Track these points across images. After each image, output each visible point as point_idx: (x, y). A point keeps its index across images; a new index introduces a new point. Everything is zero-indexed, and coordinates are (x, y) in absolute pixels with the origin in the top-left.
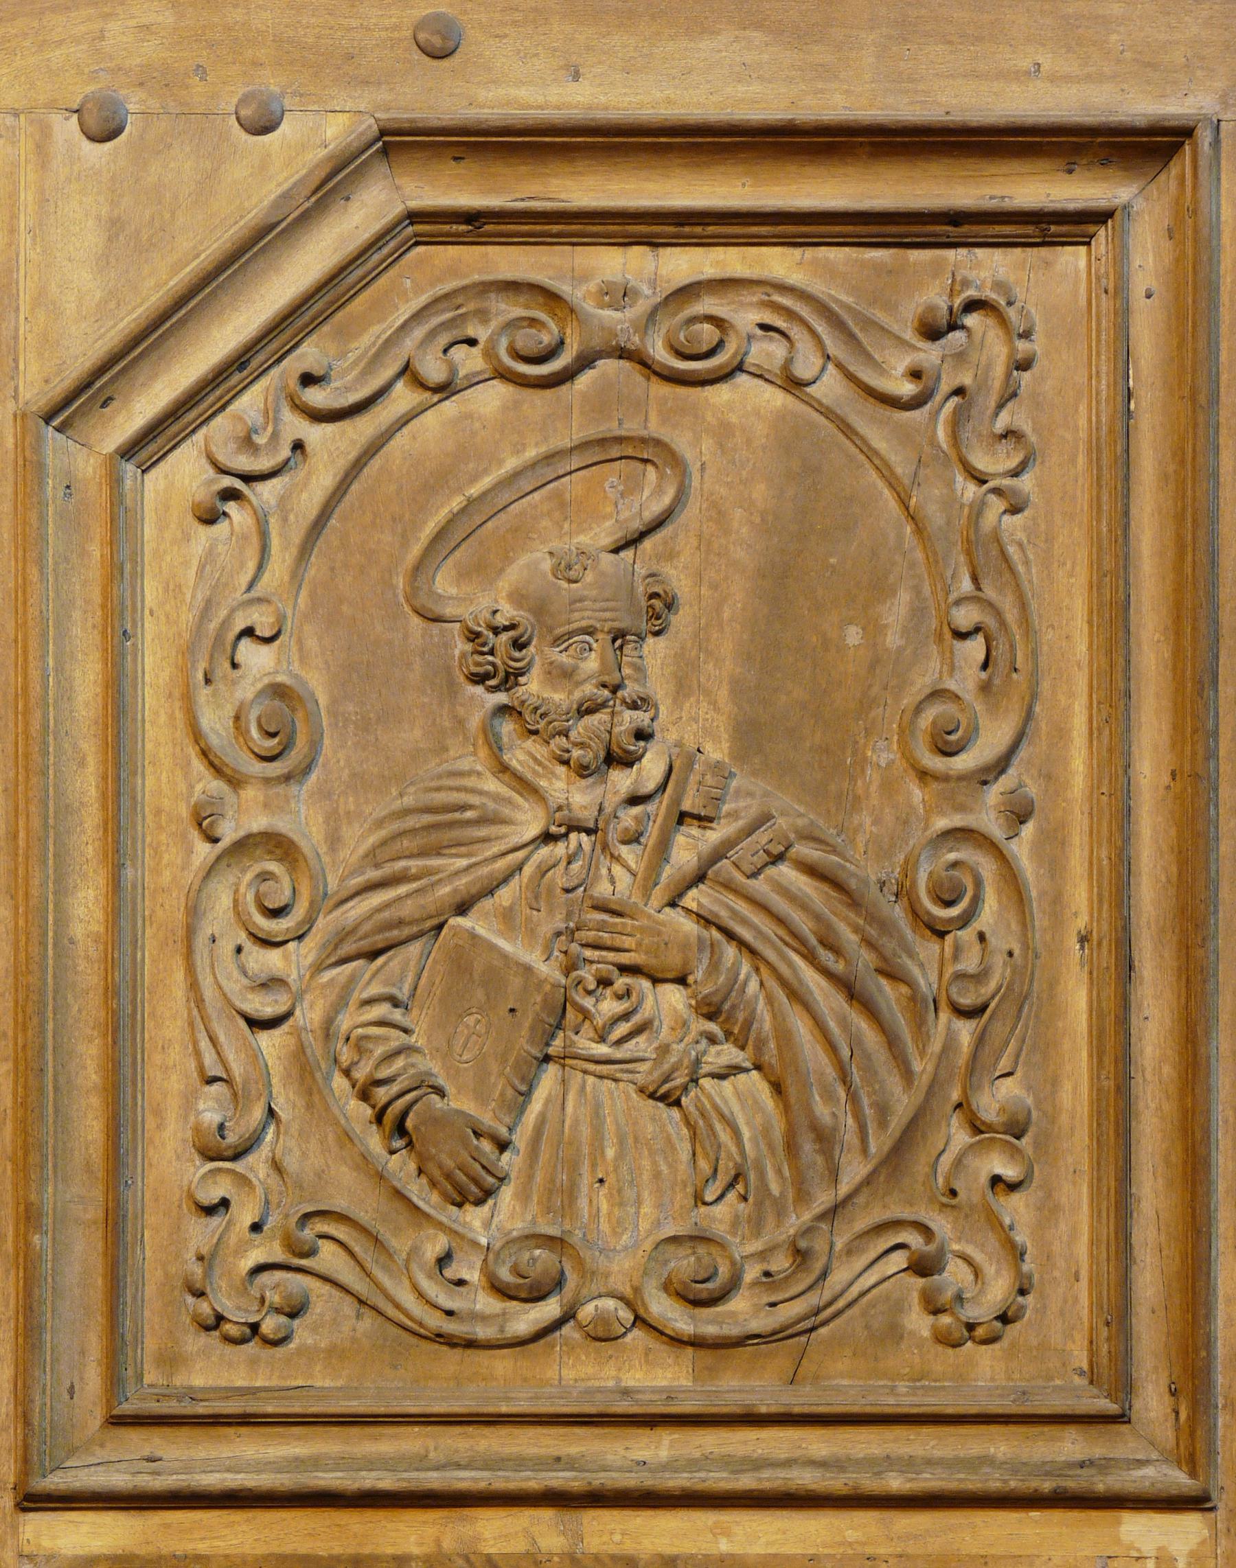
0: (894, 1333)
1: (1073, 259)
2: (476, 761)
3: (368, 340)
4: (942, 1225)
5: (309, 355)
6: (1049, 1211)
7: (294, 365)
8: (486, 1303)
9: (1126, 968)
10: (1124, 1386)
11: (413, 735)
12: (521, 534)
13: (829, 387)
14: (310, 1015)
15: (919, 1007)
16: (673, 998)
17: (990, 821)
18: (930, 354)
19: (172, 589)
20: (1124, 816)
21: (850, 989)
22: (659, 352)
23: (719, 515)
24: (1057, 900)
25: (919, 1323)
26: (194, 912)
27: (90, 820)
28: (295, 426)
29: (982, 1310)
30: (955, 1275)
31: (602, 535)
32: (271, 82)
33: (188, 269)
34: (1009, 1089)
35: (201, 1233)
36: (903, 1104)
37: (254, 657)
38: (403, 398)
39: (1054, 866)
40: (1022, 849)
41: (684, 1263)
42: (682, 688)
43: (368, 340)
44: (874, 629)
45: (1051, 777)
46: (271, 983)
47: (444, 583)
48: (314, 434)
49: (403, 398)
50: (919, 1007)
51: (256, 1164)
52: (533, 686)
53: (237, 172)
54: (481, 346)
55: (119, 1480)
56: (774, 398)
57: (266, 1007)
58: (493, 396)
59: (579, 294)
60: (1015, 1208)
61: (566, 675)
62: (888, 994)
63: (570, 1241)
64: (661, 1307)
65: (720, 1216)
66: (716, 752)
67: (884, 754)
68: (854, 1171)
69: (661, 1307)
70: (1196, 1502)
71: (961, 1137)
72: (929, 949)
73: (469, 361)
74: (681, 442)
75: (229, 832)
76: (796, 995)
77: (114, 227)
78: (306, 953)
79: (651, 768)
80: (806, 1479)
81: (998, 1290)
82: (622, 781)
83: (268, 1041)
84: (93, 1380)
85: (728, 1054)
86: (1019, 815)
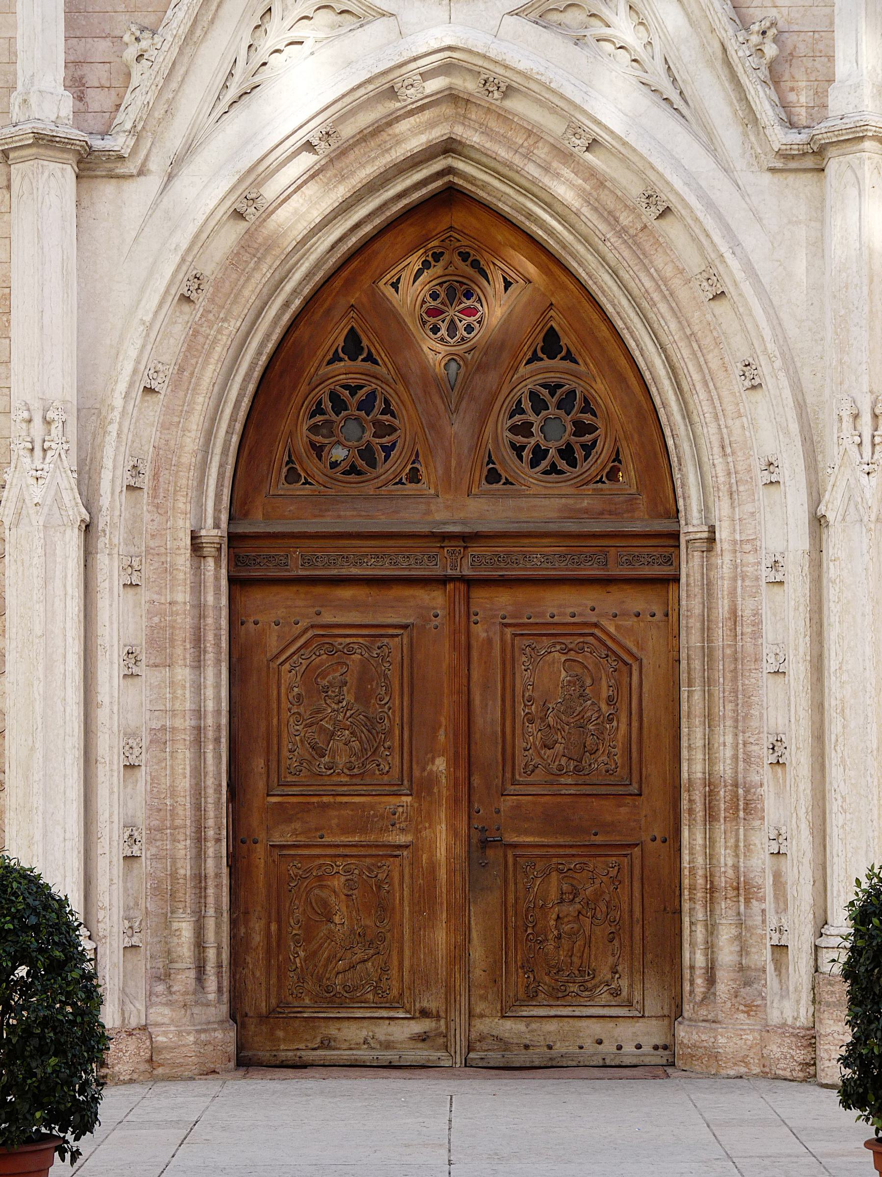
0: (374, 774)
1: (396, 639)
2: (323, 702)
3: (310, 649)
4: (380, 760)
5: (302, 651)
6: (393, 758)
7: (300, 653)
8: (324, 770)
9: (403, 728)
10: (402, 781)
11: (315, 699)
12: (328, 674)
13: (366, 655)
14: (302, 734)
15: (378, 733)
16: (347, 732)
17: (386, 710)
18: (379, 651)
19: (285, 681)
20: (402, 710)
21: (369, 731)
22: (345, 651)
23: (353, 671)
24: (394, 720)
25: (377, 772)
26: (288, 722)
27: (275, 710)
28: (301, 660)
29: (385, 771)
30: (382, 766)
31: (338, 674)
32: (298, 618)
33: (540, 232)
34: (388, 743)
35: (289, 762)
36: (375, 745)
37: (296, 689)
38: (314, 657)
39: (394, 716)
40: (390, 713)
41: (348, 765)
42: (348, 693)
43: (310, 649)
44: (372, 685)
45: (394, 704)
46: (298, 730)
47: (319, 680)
48: (303, 661)
49: (314, 657)
50: (378, 733)
51: (296, 753)
52: (330, 693)
53: (294, 629)
54: (760, 484)
55: (279, 793)
56: (359, 656)
57: (297, 733)
58: (325, 656)
59: (336, 644)
60: (389, 758)
61: (334, 692)
62: (374, 731)
63: (72, 396)
64: (345, 771)
65: (353, 759)
66: (352, 701)
67: (373, 701)
68: (369, 753)
69: (345, 771)
70: (411, 795)
71: (383, 749)
72: (379, 725)
73: (322, 652)
74: (348, 662)
75: (292, 712)
76: (362, 732)
77: (278, 636)
78: (302, 726)
79: (344, 703)
80: (363, 792)
81: (387, 768)
82: (341, 705)
83: (297, 738)
84: (276, 780)
85: (354, 739)
86: (389, 709)
